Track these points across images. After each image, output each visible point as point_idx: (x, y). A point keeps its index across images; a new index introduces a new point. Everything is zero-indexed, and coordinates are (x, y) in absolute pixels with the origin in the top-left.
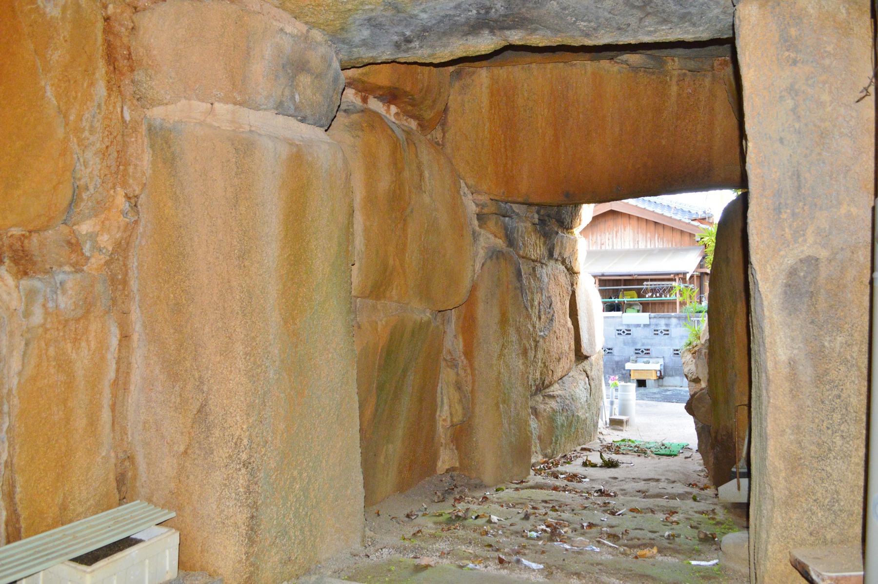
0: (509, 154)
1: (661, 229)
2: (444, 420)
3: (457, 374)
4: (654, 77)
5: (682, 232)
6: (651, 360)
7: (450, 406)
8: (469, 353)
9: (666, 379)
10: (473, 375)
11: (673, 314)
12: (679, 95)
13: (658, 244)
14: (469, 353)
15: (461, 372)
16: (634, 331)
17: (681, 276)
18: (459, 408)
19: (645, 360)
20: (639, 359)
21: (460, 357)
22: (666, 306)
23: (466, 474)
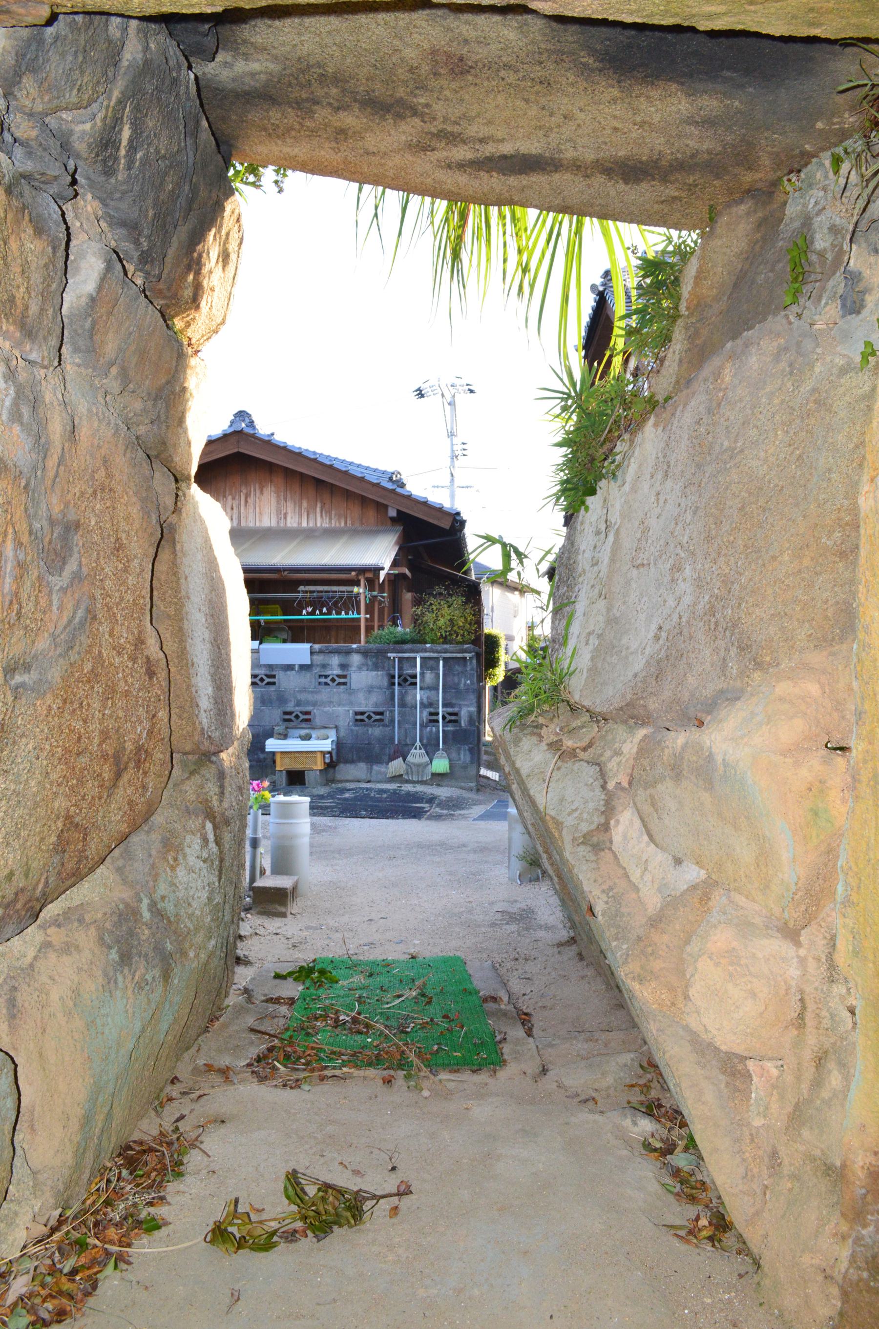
6: (314, 734)
11: (354, 646)
13: (320, 521)
16: (280, 675)
17: (369, 575)
19: (303, 732)
20: (292, 732)
22: (333, 633)
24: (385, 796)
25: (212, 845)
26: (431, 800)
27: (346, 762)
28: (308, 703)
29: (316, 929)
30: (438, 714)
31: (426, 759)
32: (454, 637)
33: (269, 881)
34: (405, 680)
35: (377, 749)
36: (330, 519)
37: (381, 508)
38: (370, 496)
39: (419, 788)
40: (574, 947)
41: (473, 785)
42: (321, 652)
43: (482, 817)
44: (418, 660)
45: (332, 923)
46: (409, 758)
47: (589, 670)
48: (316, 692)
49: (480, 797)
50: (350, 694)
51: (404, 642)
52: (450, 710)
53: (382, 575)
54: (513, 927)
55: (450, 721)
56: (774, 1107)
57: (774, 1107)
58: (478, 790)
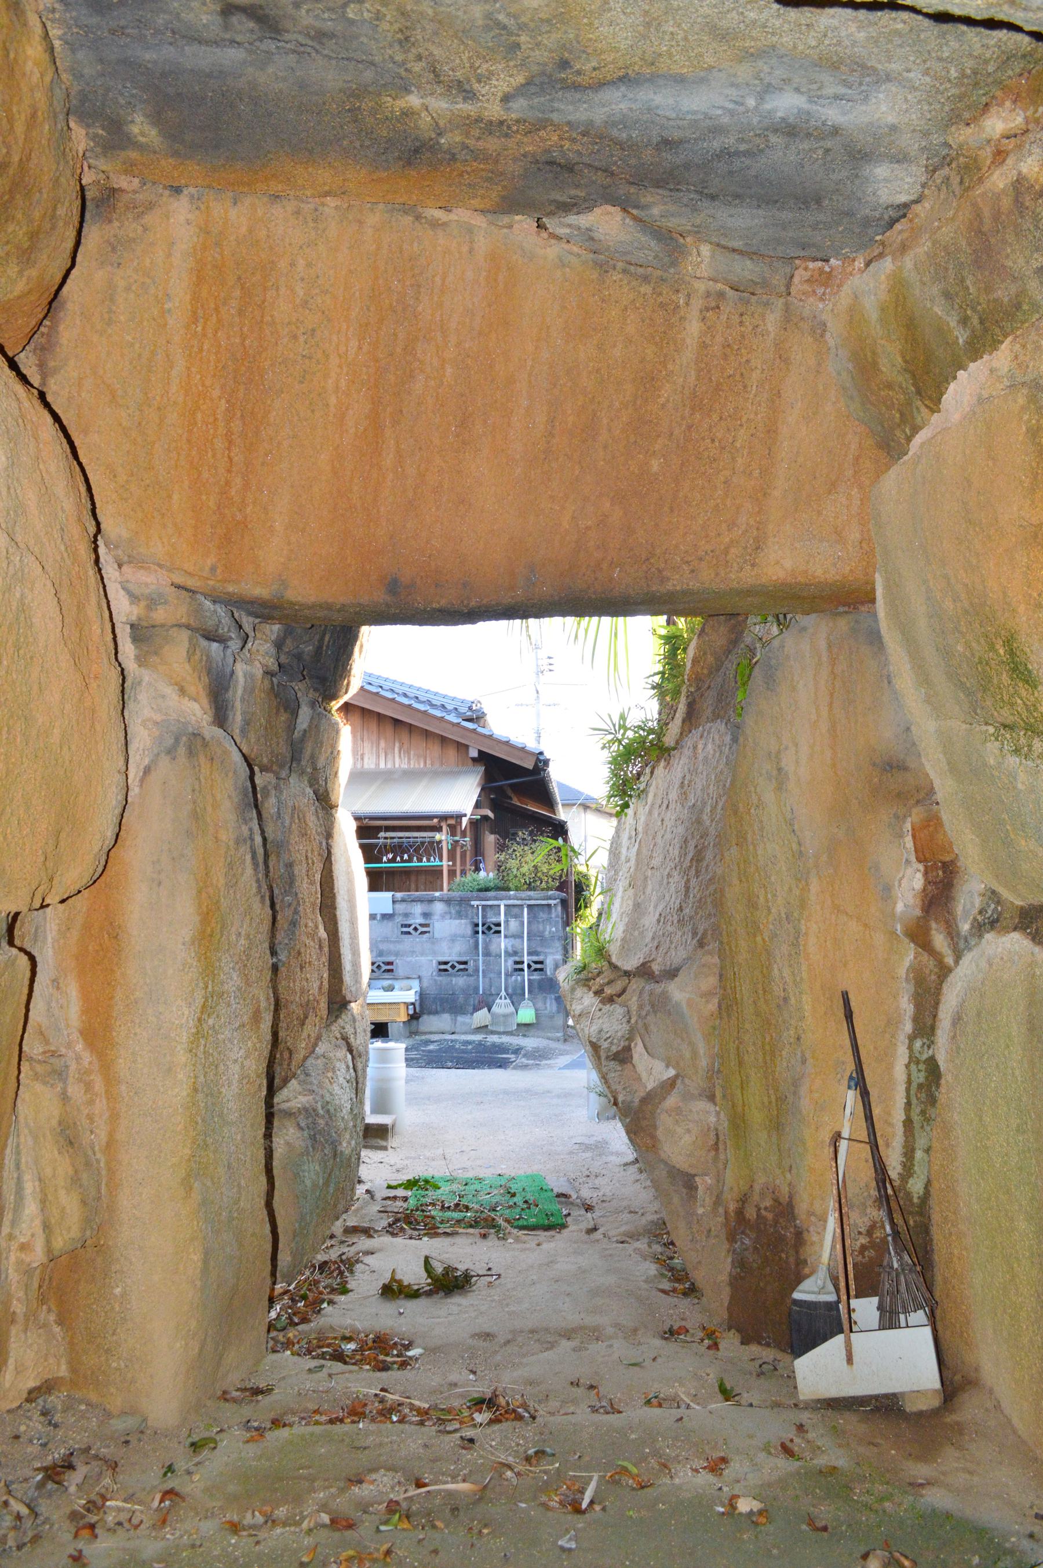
0: (238, 458)
1: (405, 736)
2: (23, 1247)
3: (65, 1097)
4: (646, 289)
5: (444, 740)
6: (397, 984)
7: (43, 1202)
8: (98, 1033)
9: (425, 1018)
10: (109, 1096)
11: (437, 894)
12: (704, 346)
13: (399, 762)
14: (98, 1033)
15: (75, 1091)
17: (452, 822)
18: (69, 1203)
21: (69, 1045)
22: (413, 878)
23: (93, 1397)
24: (470, 1047)
25: (352, 1071)
26: (517, 1051)
27: (430, 1013)
28: (390, 953)
29: (415, 1158)
30: (523, 962)
31: (512, 1009)
32: (538, 883)
33: (371, 1119)
34: (489, 928)
35: (461, 999)
36: (409, 759)
37: (462, 747)
38: (450, 737)
39: (505, 1039)
40: (637, 1165)
41: (559, 1035)
42: (403, 900)
43: (567, 1067)
44: (502, 908)
45: (428, 1154)
46: (494, 1009)
47: (622, 940)
48: (398, 942)
49: (567, 1047)
50: (433, 943)
51: (487, 889)
52: (535, 958)
53: (465, 821)
54: (589, 1154)
55: (536, 970)
56: (707, 1199)
57: (707, 1199)
58: (565, 1040)
